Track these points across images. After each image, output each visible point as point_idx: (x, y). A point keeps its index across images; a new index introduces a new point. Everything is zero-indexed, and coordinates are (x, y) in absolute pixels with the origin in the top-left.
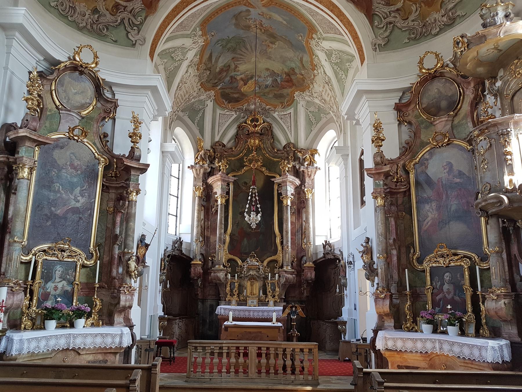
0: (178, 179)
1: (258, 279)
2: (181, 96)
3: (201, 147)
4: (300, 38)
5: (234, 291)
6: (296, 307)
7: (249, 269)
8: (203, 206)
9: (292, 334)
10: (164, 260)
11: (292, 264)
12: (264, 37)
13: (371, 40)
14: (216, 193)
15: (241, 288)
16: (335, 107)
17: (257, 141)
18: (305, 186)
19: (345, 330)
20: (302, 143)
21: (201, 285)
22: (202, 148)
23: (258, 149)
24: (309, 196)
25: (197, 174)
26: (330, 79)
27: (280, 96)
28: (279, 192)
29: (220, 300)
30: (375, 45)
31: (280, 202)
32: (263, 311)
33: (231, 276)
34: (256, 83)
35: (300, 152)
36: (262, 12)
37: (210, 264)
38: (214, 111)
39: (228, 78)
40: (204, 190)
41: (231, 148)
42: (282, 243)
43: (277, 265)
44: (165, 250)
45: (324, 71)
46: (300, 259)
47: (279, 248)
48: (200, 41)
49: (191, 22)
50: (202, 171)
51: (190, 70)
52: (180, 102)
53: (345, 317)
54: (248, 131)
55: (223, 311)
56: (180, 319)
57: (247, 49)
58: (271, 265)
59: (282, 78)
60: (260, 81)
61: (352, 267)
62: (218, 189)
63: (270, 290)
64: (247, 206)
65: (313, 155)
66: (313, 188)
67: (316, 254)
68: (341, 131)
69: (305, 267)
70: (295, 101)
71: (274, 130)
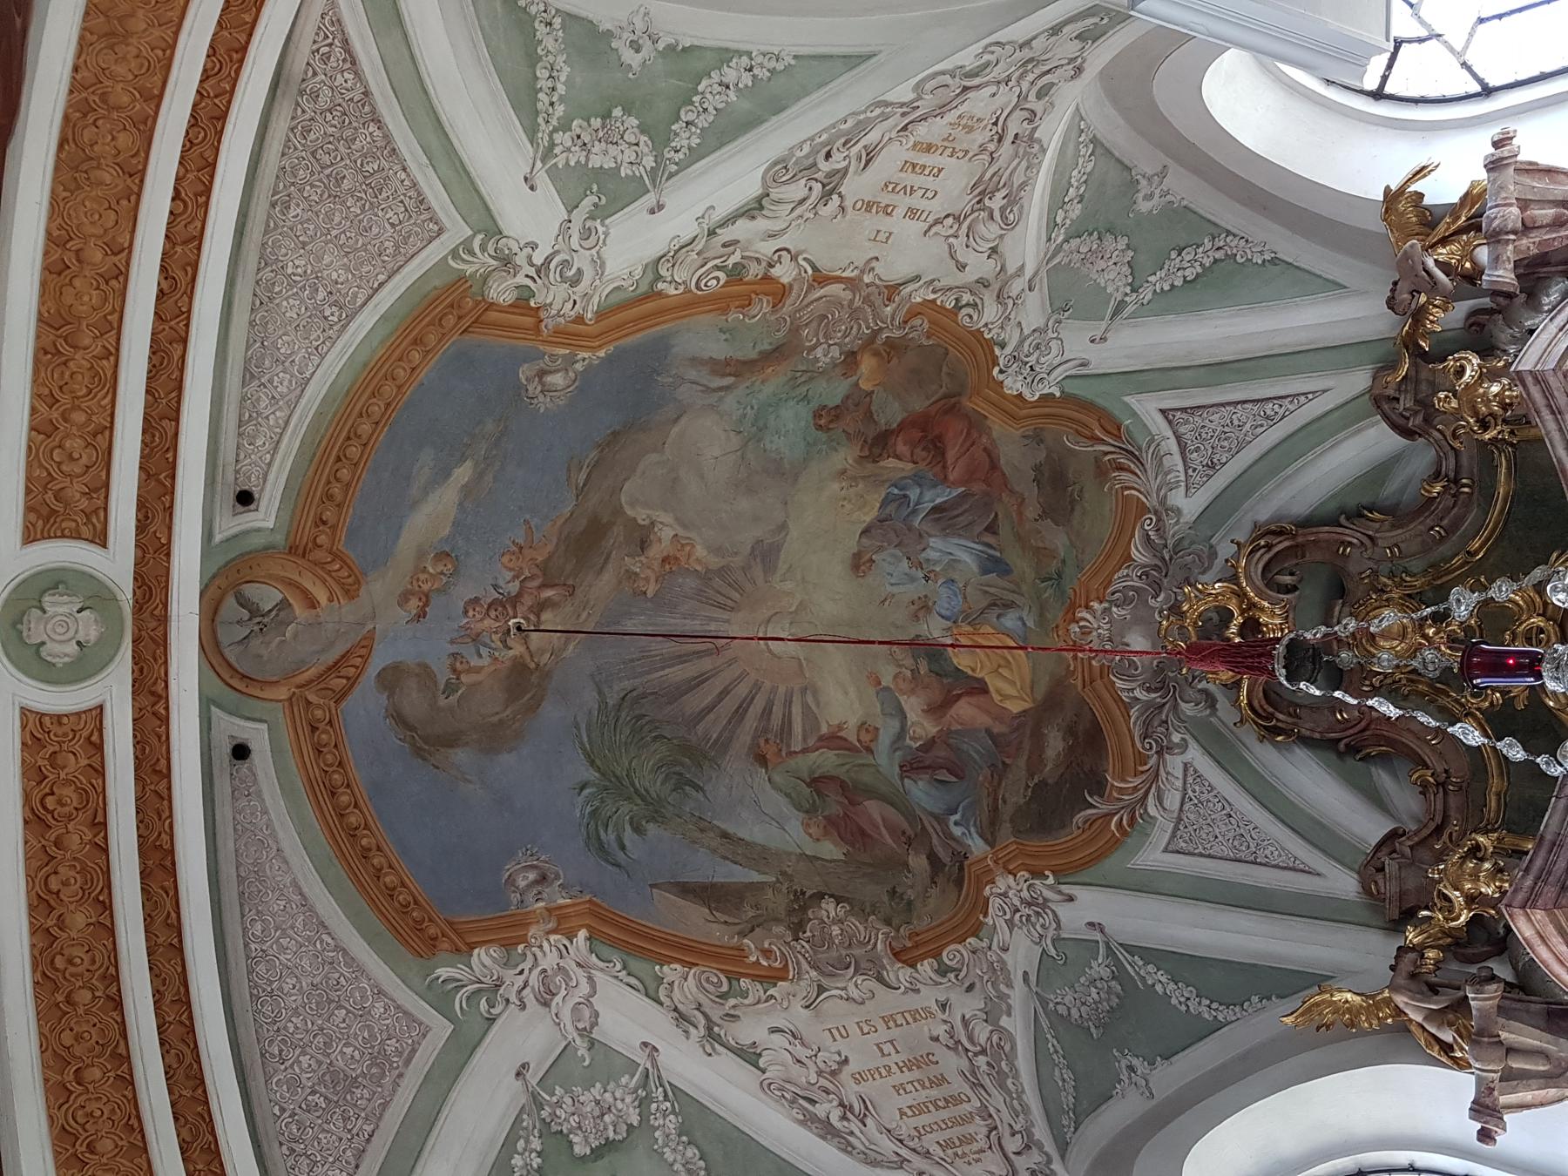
4: (557, 379)
12: (602, 586)
16: (980, 104)
20: (1362, 313)
22: (1374, 1004)
26: (782, 163)
27: (1058, 488)
35: (1419, 315)
36: (404, 598)
39: (920, 792)
41: (1424, 788)
48: (549, 960)
49: (366, 1013)
51: (750, 1030)
52: (966, 1119)
57: (700, 680)
59: (918, 480)
70: (1074, 388)
71: (1301, 508)
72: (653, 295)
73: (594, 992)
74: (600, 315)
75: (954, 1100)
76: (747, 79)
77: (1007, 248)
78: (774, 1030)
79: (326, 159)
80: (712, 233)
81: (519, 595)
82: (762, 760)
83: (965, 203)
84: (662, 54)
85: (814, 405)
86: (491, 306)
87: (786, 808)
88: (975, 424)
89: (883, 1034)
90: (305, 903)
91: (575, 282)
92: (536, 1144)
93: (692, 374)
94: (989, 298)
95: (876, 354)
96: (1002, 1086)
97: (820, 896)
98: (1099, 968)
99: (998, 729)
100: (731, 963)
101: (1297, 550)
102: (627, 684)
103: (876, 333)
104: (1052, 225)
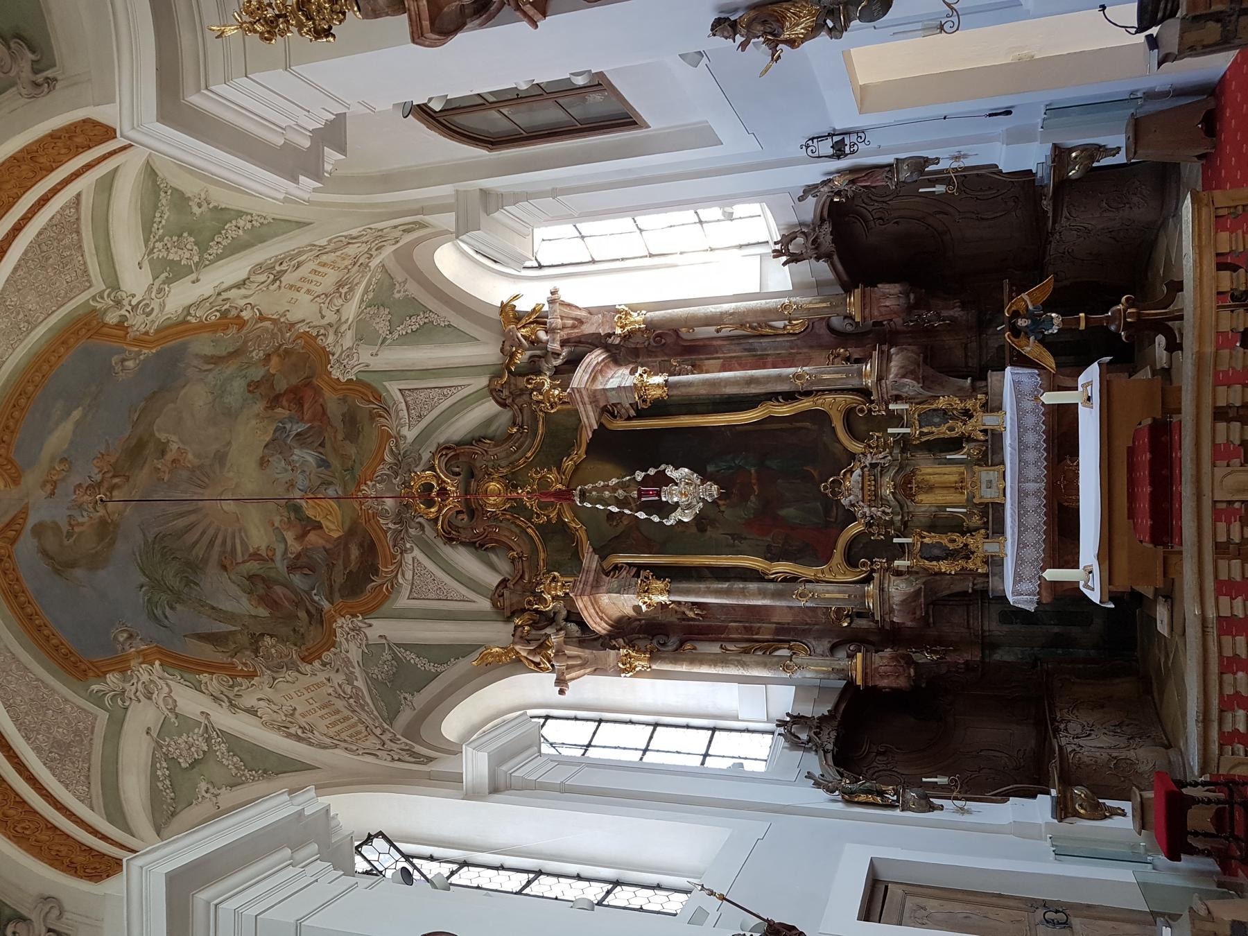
0: (600, 721)
1: (909, 469)
2: (334, 724)
3: (506, 654)
4: (130, 364)
5: (951, 546)
6: (1016, 314)
7: (875, 498)
8: (682, 643)
9: (1127, 326)
10: (851, 793)
11: (857, 361)
12: (142, 477)
13: (23, 101)
14: (637, 608)
15: (940, 523)
16: (352, 250)
17: (494, 486)
18: (609, 335)
19: (1084, 148)
20: (487, 352)
21: (936, 652)
22: (507, 650)
23: (512, 482)
24: (637, 318)
25: (582, 666)
26: (260, 265)
27: (352, 424)
28: (632, 413)
29: (984, 592)
30: (37, 85)
31: (659, 408)
32: (1022, 447)
33: (901, 557)
34: (313, 493)
35: (512, 356)
36: (43, 485)
37: (862, 623)
38: (402, 615)
39: (297, 579)
40: (631, 644)
41: (513, 560)
42: (789, 397)
43: (861, 411)
44: (817, 784)
45: (238, 286)
46: (841, 337)
47: (805, 404)
48: (145, 677)
49: (62, 711)
50: (571, 651)
51: (249, 700)
53: (1031, 157)
54: (458, 512)
55: (1025, 586)
56: (1056, 731)
57: (191, 527)
58: (862, 427)
59: (291, 419)
60: (306, 482)
61: (854, 138)
62: (624, 603)
63: (944, 428)
64: (642, 515)
65: (519, 317)
66: (613, 310)
67: (820, 285)
68: (422, 226)
69: (864, 318)
70: (361, 376)
71: (456, 438)
72: (185, 322)
73: (171, 691)
74: (157, 331)
75: (346, 719)
76: (249, 226)
77: (343, 311)
78: (260, 699)
79: (45, 248)
80: (219, 294)
81: (102, 481)
82: (224, 568)
83: (331, 289)
84: (211, 210)
85: (249, 380)
86: (105, 325)
87: (240, 593)
88: (318, 391)
89: (307, 696)
90: (14, 657)
91: (148, 315)
92: (165, 765)
93: (195, 362)
94: (331, 331)
95: (279, 356)
96: (364, 710)
97: (262, 635)
98: (386, 656)
99: (328, 546)
100: (230, 670)
101: (456, 456)
102: (156, 529)
103: (281, 345)
104: (362, 301)
